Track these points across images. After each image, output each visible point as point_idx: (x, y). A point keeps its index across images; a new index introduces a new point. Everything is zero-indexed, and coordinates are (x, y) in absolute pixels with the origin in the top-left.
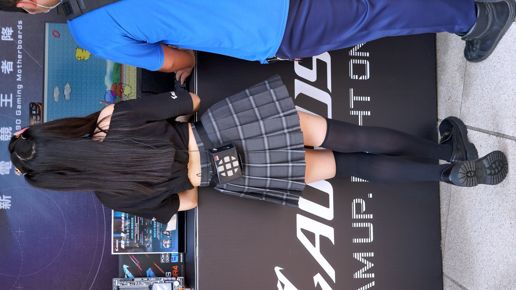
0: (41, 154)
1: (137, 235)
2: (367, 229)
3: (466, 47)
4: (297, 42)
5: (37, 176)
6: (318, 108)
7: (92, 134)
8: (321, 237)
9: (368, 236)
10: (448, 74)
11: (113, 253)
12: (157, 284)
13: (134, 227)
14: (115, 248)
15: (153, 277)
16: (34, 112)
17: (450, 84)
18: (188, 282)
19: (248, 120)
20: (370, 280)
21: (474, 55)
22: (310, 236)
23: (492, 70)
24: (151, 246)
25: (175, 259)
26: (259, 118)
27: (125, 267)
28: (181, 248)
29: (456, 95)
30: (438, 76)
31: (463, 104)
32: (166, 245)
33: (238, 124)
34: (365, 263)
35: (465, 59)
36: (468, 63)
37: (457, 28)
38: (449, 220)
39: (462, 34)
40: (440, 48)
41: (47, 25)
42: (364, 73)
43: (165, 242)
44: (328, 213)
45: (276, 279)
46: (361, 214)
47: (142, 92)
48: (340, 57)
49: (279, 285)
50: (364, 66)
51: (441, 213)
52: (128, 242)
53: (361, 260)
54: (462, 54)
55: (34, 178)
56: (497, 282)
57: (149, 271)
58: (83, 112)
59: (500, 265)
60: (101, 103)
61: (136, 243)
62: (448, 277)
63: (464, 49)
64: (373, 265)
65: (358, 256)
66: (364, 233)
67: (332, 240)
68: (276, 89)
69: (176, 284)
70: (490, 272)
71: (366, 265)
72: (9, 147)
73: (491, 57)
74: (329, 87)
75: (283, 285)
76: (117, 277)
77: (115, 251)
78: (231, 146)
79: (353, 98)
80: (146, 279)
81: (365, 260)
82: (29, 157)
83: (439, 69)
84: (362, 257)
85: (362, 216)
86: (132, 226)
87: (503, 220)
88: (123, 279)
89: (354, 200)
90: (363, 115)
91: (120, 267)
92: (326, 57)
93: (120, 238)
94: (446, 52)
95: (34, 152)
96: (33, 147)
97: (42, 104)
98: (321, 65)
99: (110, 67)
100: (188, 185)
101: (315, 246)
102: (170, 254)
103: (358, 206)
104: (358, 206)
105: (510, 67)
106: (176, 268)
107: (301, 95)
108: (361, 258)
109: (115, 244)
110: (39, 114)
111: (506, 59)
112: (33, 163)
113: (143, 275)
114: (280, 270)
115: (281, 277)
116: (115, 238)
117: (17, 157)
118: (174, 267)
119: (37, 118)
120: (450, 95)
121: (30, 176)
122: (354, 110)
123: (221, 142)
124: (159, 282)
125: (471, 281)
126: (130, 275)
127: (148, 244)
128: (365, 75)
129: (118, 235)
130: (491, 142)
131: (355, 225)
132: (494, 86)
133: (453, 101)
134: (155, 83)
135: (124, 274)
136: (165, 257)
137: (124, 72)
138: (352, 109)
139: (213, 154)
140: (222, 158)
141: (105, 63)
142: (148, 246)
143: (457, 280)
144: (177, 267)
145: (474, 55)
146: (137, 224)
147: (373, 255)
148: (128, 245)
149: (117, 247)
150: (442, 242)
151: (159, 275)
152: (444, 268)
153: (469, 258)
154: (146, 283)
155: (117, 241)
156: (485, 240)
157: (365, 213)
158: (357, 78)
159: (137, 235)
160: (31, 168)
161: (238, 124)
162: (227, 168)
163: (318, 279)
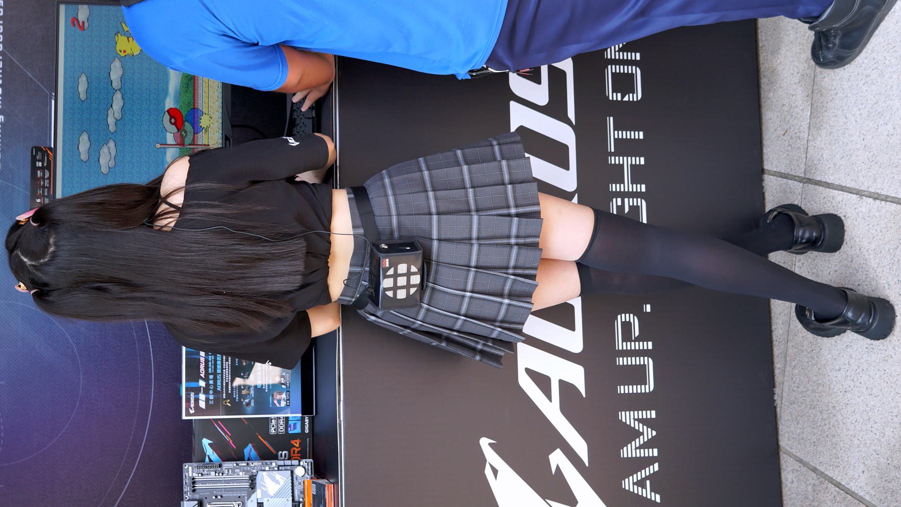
0: (61, 252)
1: (227, 384)
2: (643, 368)
3: (814, 42)
4: (519, 44)
5: (55, 294)
6: (554, 152)
7: (153, 217)
8: (562, 383)
9: (643, 381)
10: (781, 90)
11: (184, 417)
12: (264, 473)
13: (222, 369)
14: (187, 410)
15: (256, 460)
16: (39, 164)
17: (786, 108)
18: (323, 468)
19: (453, 207)
20: (649, 461)
21: (830, 56)
22: (542, 381)
23: (863, 82)
24: (252, 404)
25: (295, 428)
26: (473, 207)
27: (206, 442)
28: (307, 408)
29: (797, 127)
30: (763, 94)
31: (811, 143)
32: (279, 401)
33: (434, 210)
34: (641, 430)
35: (812, 63)
36: (819, 69)
37: (801, 10)
38: (790, 351)
39: (810, 19)
40: (766, 43)
41: (62, 8)
42: (632, 90)
43: (278, 397)
44: (574, 341)
45: (483, 460)
46: (631, 341)
47: (233, 126)
48: (590, 66)
49: (488, 472)
50: (631, 77)
51: (774, 338)
52: (211, 397)
53: (632, 425)
54: (808, 53)
55: (50, 298)
56: (881, 460)
57: (249, 450)
58: (142, 179)
59: (887, 429)
60: (158, 146)
61: (226, 399)
62: (790, 455)
63: (810, 46)
64: (654, 433)
65: (628, 417)
66: (638, 375)
67: (582, 389)
68: (512, 162)
69: (299, 471)
70: (868, 442)
71: (642, 434)
72: (7, 243)
73: (860, 59)
74: (571, 114)
75: (495, 472)
76: (190, 460)
77: (188, 414)
78: (414, 247)
79: (613, 135)
80: (243, 464)
81: (641, 425)
82: (43, 258)
83: (763, 81)
84: (635, 420)
85: (633, 346)
86: (219, 367)
87: (890, 348)
88: (201, 464)
89: (619, 317)
90: (631, 165)
91: (195, 442)
92: (567, 65)
93: (197, 390)
94: (775, 51)
95: (52, 249)
96: (52, 241)
97: (54, 150)
98: (557, 77)
99: (174, 81)
100: (324, 297)
101: (550, 400)
102: (287, 418)
103: (627, 326)
104: (627, 326)
105: (895, 76)
106: (296, 443)
107: (522, 129)
108: (632, 421)
109: (188, 400)
110: (48, 167)
111: (887, 62)
112: (51, 269)
113: (238, 457)
114: (490, 444)
115: (492, 457)
116: (188, 390)
117: (21, 260)
118: (293, 442)
119: (44, 175)
120: (786, 127)
121: (42, 293)
122: (615, 154)
123: (396, 235)
124: (267, 468)
125: (833, 460)
126: (214, 456)
127: (247, 401)
128: (633, 93)
129: (193, 385)
130: (864, 210)
131: (621, 361)
132: (866, 110)
133: (792, 138)
134: (256, 114)
135: (203, 454)
136: (277, 424)
137: (200, 92)
138: (612, 154)
139: (381, 255)
140: (394, 265)
141: (166, 75)
142: (248, 404)
143: (807, 459)
144: (298, 441)
145: (830, 56)
146: (228, 364)
147: (654, 416)
148: (211, 402)
149: (192, 405)
150: (777, 390)
151: (266, 456)
152: (781, 438)
153: (829, 418)
154: (244, 471)
155: (192, 395)
156: (858, 384)
157: (638, 339)
158: (619, 99)
159: (227, 384)
160: (45, 278)
161: (434, 210)
162: (405, 278)
163: (557, 459)
